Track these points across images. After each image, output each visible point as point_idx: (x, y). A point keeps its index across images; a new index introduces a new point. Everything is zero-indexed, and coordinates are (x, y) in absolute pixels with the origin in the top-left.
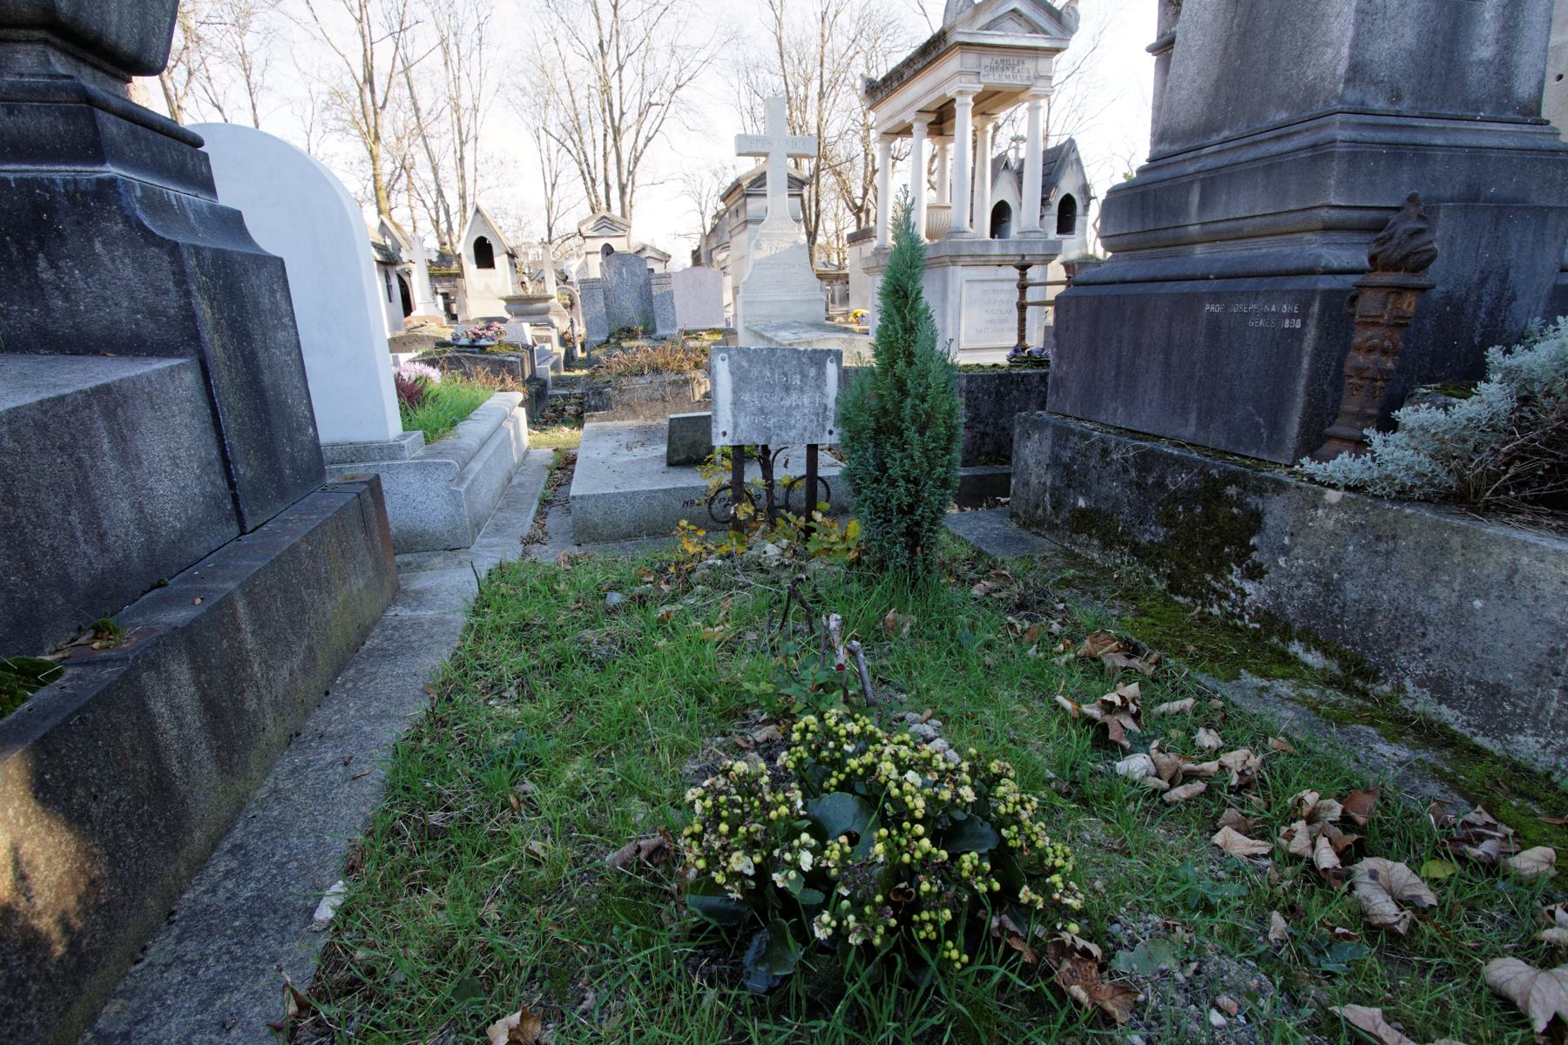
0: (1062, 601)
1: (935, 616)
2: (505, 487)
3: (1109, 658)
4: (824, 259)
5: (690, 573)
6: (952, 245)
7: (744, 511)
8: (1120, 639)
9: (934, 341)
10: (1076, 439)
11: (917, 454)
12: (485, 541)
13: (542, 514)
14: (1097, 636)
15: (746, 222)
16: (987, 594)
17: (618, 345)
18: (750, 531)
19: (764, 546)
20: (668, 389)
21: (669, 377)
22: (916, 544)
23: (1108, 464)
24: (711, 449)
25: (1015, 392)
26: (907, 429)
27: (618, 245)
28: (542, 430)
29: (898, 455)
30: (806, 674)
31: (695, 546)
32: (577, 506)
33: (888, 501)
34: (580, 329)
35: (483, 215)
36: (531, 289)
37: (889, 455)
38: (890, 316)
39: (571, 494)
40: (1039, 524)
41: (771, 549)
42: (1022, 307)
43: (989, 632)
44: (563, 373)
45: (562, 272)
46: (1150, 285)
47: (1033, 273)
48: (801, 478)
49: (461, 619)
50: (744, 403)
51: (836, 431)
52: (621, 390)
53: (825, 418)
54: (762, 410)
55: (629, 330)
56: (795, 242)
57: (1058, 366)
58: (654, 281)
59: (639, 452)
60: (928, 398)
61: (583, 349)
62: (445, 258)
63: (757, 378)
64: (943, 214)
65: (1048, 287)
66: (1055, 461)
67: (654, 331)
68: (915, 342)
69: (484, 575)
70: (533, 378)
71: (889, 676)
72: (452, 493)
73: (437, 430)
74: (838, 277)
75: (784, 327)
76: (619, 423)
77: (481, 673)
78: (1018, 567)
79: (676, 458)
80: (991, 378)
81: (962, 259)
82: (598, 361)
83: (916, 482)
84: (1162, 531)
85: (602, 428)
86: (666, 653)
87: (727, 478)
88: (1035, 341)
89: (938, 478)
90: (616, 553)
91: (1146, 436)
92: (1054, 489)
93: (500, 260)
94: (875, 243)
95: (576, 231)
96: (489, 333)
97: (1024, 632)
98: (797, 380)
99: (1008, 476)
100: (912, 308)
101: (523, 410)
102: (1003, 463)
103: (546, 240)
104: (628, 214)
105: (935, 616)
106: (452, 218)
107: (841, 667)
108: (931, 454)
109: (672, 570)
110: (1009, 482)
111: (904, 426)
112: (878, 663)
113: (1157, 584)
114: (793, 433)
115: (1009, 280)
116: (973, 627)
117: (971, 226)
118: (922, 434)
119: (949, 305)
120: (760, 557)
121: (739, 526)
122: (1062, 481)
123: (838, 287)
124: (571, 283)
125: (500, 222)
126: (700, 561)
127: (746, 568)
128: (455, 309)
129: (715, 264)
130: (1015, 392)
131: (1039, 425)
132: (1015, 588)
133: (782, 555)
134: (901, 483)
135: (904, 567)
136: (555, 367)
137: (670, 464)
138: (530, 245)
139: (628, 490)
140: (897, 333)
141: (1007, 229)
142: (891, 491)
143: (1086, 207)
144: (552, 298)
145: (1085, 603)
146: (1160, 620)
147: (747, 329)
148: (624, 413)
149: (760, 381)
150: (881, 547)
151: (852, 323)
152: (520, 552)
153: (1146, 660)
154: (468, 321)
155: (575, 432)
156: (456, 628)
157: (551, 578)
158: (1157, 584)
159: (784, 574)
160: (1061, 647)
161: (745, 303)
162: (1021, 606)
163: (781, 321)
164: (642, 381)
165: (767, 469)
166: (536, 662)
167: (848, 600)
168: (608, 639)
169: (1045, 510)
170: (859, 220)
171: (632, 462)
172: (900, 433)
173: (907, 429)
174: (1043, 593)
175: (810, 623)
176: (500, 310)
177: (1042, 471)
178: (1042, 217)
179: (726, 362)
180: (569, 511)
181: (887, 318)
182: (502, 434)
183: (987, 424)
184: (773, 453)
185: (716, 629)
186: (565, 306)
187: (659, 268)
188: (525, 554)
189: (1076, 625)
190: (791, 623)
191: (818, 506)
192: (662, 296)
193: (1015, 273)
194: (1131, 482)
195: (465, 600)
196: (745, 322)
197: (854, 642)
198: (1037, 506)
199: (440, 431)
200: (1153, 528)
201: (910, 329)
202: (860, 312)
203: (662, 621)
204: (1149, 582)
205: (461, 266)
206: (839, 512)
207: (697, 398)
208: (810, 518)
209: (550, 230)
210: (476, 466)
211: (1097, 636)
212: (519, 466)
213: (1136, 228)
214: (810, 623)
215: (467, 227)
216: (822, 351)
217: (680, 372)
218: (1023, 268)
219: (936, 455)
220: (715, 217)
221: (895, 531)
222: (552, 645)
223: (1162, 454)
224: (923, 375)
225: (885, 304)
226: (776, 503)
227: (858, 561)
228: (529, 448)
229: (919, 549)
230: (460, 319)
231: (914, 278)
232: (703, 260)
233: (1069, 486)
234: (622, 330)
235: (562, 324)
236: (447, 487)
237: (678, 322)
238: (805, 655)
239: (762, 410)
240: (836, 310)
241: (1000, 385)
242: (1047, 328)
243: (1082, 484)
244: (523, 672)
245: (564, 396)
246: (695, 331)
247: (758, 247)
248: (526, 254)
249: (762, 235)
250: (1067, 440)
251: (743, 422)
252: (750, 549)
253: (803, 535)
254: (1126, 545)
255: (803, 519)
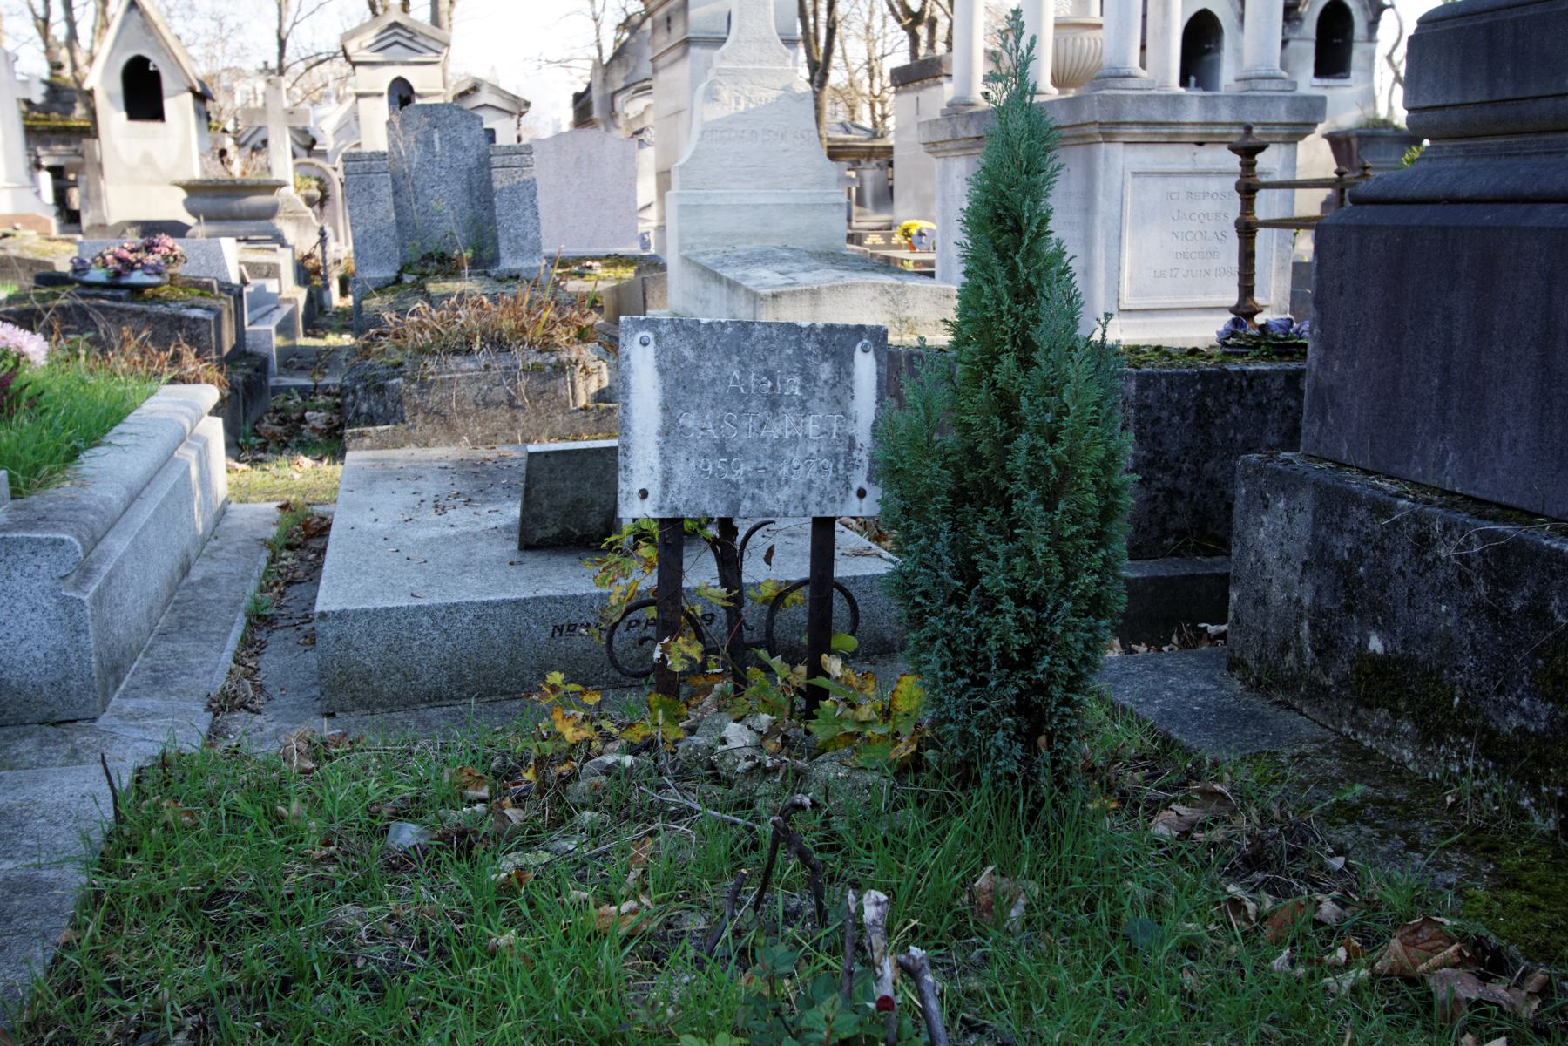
0: (1340, 851)
1: (1078, 882)
2: (174, 587)
3: (1442, 979)
4: (843, 117)
5: (565, 783)
6: (1104, 101)
7: (681, 652)
8: (1463, 937)
9: (1073, 319)
10: (1362, 513)
11: (1040, 548)
12: (130, 705)
13: (251, 646)
14: (1416, 930)
15: (687, 42)
16: (1185, 835)
17: (420, 290)
18: (692, 695)
19: (721, 727)
20: (522, 383)
21: (525, 357)
22: (1036, 730)
23: (1430, 566)
24: (611, 523)
25: (1235, 409)
26: (1019, 495)
27: (422, 80)
28: (254, 463)
29: (1000, 548)
30: (813, 1017)
31: (577, 726)
32: (330, 634)
33: (981, 640)
34: (341, 249)
35: (143, 13)
36: (237, 167)
37: (980, 548)
38: (985, 266)
39: (319, 607)
40: (1289, 685)
41: (737, 735)
42: (1247, 230)
43: (1189, 919)
44: (302, 341)
45: (305, 132)
46: (1507, 208)
47: (1269, 162)
48: (803, 583)
49: (75, 880)
50: (684, 431)
51: (874, 493)
52: (424, 385)
53: (851, 465)
54: (721, 448)
55: (443, 259)
56: (787, 88)
57: (1324, 364)
58: (496, 161)
59: (461, 517)
60: (1063, 435)
61: (344, 292)
62: (60, 94)
63: (713, 381)
64: (1087, 39)
65: (1298, 192)
66: (1319, 559)
67: (495, 260)
68: (1036, 321)
69: (126, 780)
70: (241, 353)
71: (982, 1014)
72: (65, 602)
73: (37, 467)
74: (870, 153)
75: (763, 258)
76: (419, 453)
77: (114, 1003)
78: (1247, 776)
79: (539, 534)
80: (1187, 380)
81: (1123, 130)
82: (377, 321)
83: (1037, 603)
84: (1543, 709)
85: (383, 463)
86: (517, 962)
87: (648, 581)
88: (1273, 302)
89: (1081, 596)
90: (410, 734)
91: (1506, 512)
92: (1318, 614)
93: (177, 105)
94: (948, 91)
95: (336, 48)
96: (151, 259)
97: (1262, 918)
98: (793, 386)
99: (1224, 581)
100: (1029, 251)
101: (218, 423)
102: (1211, 553)
103: (274, 64)
104: (444, 17)
105: (1078, 882)
106: (77, 14)
107: (885, 1003)
108: (1068, 547)
109: (529, 775)
110: (1228, 596)
111: (1013, 489)
112: (959, 985)
113: (1538, 820)
114: (784, 494)
115: (1220, 173)
116: (1156, 907)
117: (1143, 65)
118: (1050, 506)
119: (1098, 222)
120: (711, 750)
121: (667, 683)
122: (1335, 599)
123: (870, 174)
124: (323, 154)
125: (178, 26)
126: (588, 758)
127: (683, 775)
128: (75, 198)
129: (621, 121)
130: (1235, 409)
131: (1286, 483)
132: (1240, 820)
133: (759, 747)
134: (1007, 604)
135: (1012, 777)
136: (285, 328)
137: (527, 545)
138: (239, 74)
139: (438, 600)
140: (999, 302)
141: (1215, 66)
142: (985, 620)
143: (1373, 25)
144: (281, 185)
145: (1390, 856)
146: (1546, 896)
147: (686, 260)
148: (428, 430)
149: (719, 388)
150: (965, 736)
151: (899, 247)
152: (204, 727)
153: (1519, 984)
154: (102, 227)
155: (325, 466)
156: (62, 899)
157: (271, 789)
158: (1538, 820)
159: (763, 789)
160: (1341, 953)
161: (683, 207)
162: (1255, 861)
163: (756, 245)
164: (468, 365)
165: (730, 564)
166: (232, 978)
167: (895, 845)
168: (391, 928)
169: (1300, 655)
170: (915, 39)
171: (447, 540)
172: (1006, 503)
173: (1019, 495)
174: (1299, 833)
175: (818, 895)
176: (173, 207)
177: (1294, 577)
178: (1285, 43)
179: (651, 349)
180: (312, 640)
181: (978, 268)
182: (174, 476)
183: (1179, 473)
184: (742, 534)
185: (625, 907)
186: (310, 202)
187: (506, 133)
188: (215, 733)
189: (1372, 905)
190: (780, 900)
191: (834, 644)
192: (512, 190)
193: (1235, 162)
194: (1477, 605)
195: (86, 839)
196: (682, 247)
197: (915, 951)
198: (1284, 649)
199: (45, 470)
200: (1525, 702)
201: (1025, 294)
202: (917, 224)
203: (507, 889)
204: (1520, 814)
205: (92, 113)
206: (876, 650)
207: (582, 402)
208: (817, 669)
209: (282, 44)
210: (118, 545)
211: (1416, 930)
212: (205, 541)
213: (1477, 94)
214: (818, 895)
215: (111, 34)
216: (846, 328)
217: (547, 347)
218: (1248, 153)
219: (1078, 548)
220: (623, 26)
221: (994, 704)
222: (271, 940)
223: (1539, 551)
224: (1052, 388)
225: (975, 242)
226: (747, 635)
227: (915, 763)
228: (227, 502)
229: (1042, 740)
230: (86, 221)
231: (1035, 193)
232: (596, 114)
233: (1349, 609)
234: (429, 257)
235: (302, 239)
236: (54, 592)
237: (545, 241)
238: (808, 971)
239: (721, 448)
240: (869, 219)
241: (1204, 394)
242: (1297, 266)
243: (1376, 607)
244: (207, 999)
245: (303, 390)
246: (579, 260)
247: (712, 96)
248: (230, 91)
249: (719, 73)
250: (1344, 514)
251: (684, 471)
252: (692, 731)
253: (801, 702)
254: (1469, 735)
255: (802, 669)
